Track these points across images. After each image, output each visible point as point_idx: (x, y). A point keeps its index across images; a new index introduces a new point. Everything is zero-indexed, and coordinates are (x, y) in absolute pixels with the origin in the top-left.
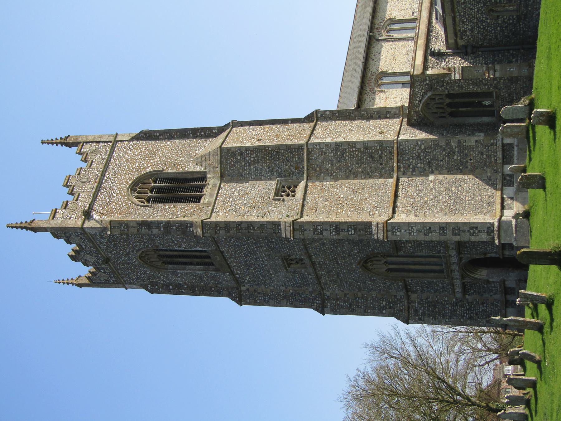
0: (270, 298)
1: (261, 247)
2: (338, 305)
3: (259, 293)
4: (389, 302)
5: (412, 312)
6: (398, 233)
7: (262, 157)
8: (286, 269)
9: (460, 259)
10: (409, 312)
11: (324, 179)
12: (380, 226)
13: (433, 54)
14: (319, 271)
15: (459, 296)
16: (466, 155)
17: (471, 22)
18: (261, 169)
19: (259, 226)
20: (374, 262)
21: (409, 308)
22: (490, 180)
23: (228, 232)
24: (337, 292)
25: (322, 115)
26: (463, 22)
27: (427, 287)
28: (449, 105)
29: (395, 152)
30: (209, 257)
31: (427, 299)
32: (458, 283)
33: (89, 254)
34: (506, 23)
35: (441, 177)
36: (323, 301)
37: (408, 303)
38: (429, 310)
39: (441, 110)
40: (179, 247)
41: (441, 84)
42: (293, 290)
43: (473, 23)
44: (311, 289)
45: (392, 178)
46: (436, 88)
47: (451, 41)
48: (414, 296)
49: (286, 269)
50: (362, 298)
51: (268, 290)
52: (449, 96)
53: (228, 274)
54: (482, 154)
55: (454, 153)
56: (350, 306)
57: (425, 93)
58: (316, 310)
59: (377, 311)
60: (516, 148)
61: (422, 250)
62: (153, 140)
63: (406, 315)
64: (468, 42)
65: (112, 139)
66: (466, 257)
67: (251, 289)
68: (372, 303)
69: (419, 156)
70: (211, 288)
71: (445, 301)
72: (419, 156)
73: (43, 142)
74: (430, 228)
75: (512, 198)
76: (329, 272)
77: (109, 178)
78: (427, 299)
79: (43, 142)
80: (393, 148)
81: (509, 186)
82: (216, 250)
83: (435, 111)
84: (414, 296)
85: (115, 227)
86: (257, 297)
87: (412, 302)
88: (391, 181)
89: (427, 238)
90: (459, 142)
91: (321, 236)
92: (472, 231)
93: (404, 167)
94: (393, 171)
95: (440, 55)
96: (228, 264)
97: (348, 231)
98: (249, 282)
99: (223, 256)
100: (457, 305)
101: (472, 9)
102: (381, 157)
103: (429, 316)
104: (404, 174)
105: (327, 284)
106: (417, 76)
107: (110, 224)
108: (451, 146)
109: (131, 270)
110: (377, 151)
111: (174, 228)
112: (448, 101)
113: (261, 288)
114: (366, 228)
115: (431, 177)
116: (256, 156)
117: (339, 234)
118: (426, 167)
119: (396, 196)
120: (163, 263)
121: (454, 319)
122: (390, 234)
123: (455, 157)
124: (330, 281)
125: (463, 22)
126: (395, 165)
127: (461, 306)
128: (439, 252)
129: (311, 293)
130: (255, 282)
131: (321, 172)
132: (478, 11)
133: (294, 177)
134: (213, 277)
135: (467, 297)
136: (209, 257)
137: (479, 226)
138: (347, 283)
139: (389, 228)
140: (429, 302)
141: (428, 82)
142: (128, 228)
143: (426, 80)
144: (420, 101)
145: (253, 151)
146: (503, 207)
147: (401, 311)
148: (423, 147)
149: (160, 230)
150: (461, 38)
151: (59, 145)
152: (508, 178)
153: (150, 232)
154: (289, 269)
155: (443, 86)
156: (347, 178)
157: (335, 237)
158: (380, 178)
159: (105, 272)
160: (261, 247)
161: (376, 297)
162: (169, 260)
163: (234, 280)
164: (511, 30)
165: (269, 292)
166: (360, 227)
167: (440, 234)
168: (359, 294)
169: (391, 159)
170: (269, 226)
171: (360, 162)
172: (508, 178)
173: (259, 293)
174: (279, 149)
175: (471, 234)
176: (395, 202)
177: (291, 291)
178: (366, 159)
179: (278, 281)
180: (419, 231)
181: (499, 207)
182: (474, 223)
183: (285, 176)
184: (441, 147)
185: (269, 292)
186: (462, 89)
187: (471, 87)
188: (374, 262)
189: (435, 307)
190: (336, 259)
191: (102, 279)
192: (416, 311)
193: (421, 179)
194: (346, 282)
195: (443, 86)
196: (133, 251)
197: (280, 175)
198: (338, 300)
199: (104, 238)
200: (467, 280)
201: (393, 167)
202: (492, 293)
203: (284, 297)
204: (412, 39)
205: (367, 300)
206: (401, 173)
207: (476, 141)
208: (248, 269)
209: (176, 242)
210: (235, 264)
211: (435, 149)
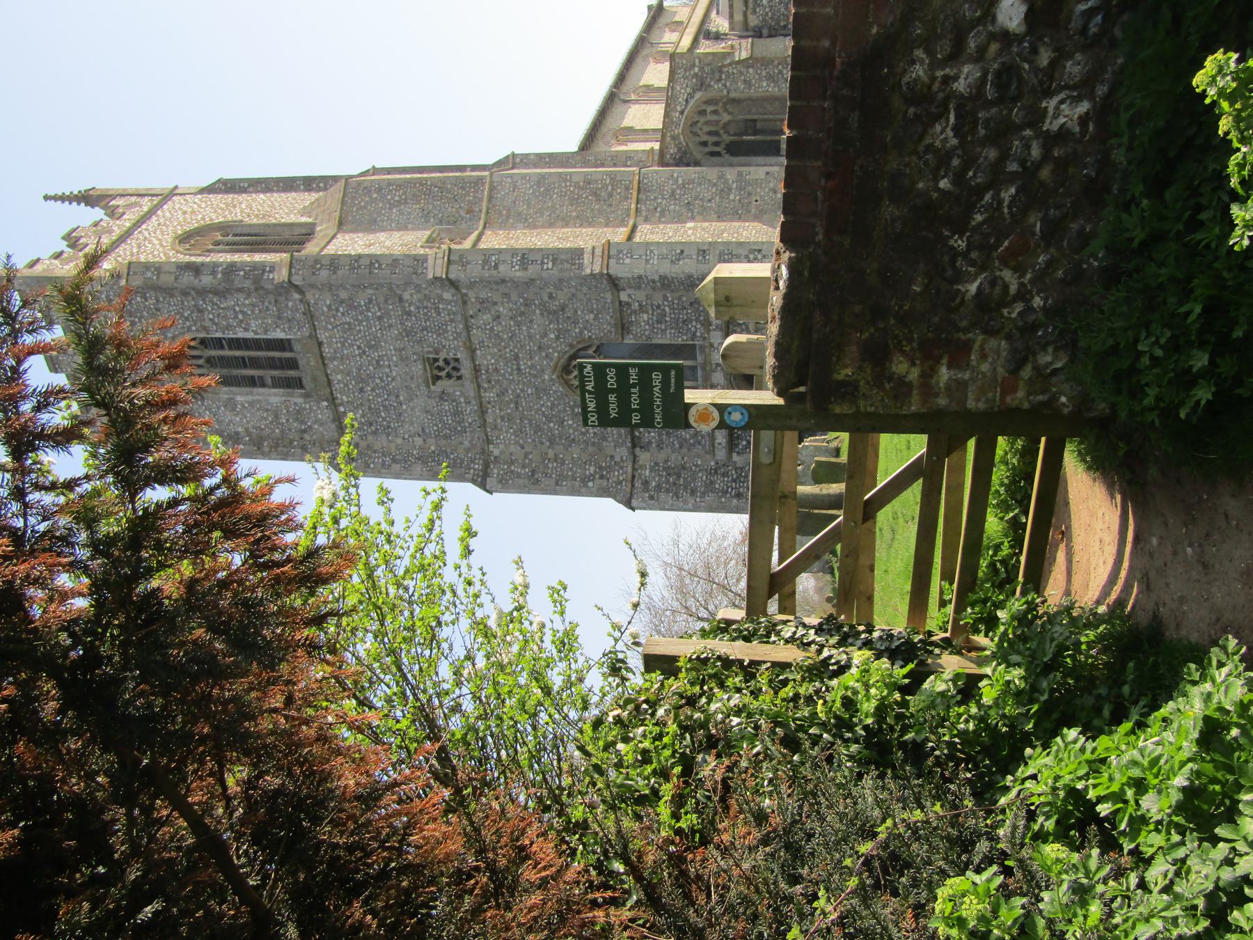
0: (394, 461)
1: (390, 326)
2: (512, 472)
3: (375, 452)
4: (601, 468)
5: (638, 484)
6: (627, 261)
7: (414, 195)
8: (428, 387)
10: (633, 486)
11: (514, 227)
12: (598, 251)
14: (485, 390)
15: (721, 454)
16: (750, 194)
18: (410, 214)
19: (390, 261)
21: (633, 477)
23: (335, 273)
24: (512, 448)
25: (522, 161)
29: (636, 187)
31: (666, 461)
36: (486, 466)
37: (634, 469)
38: (667, 482)
39: (715, 139)
41: (717, 75)
42: (437, 445)
45: (626, 226)
46: (709, 86)
47: (738, 17)
48: (644, 457)
49: (428, 387)
50: (555, 460)
51: (393, 446)
53: (325, 403)
54: (775, 192)
55: (730, 189)
56: (533, 475)
57: (691, 96)
58: (474, 482)
59: (577, 484)
61: (664, 331)
62: (235, 193)
63: (628, 490)
64: (764, 20)
68: (571, 469)
69: (673, 194)
70: (291, 441)
71: (697, 466)
72: (673, 194)
73: (47, 198)
74: (682, 252)
76: (503, 393)
78: (666, 461)
79: (47, 198)
80: (631, 182)
82: (310, 336)
83: (705, 138)
84: (644, 457)
85: (135, 273)
86: (370, 457)
87: (641, 467)
90: (740, 174)
93: (648, 210)
94: (628, 216)
95: (717, 37)
96: (327, 375)
97: (543, 263)
99: (321, 353)
100: (716, 473)
102: (610, 195)
103: (668, 491)
104: (646, 220)
105: (495, 427)
106: (682, 55)
107: (129, 268)
108: (726, 181)
110: (605, 186)
111: (242, 273)
113: (381, 442)
115: (690, 225)
116: (405, 193)
117: (526, 269)
118: (684, 210)
121: (710, 498)
122: (612, 262)
123: (732, 197)
124: (502, 418)
126: (633, 206)
127: (724, 475)
129: (468, 450)
130: (371, 424)
131: (508, 217)
133: (464, 226)
134: (299, 414)
135: (735, 457)
137: (764, 247)
138: (531, 425)
139: (613, 252)
140: (669, 468)
141: (696, 70)
143: (694, 66)
144: (682, 113)
145: (400, 186)
147: (620, 483)
148: (680, 181)
149: (215, 277)
150: (754, 12)
151: (75, 204)
154: (433, 388)
155: (720, 80)
156: (551, 225)
157: (518, 274)
158: (607, 226)
160: (390, 326)
161: (579, 458)
163: (334, 420)
166: (563, 257)
168: (551, 454)
169: (626, 198)
170: (407, 263)
171: (574, 201)
173: (375, 452)
174: (444, 183)
177: (433, 448)
179: (412, 423)
180: (663, 257)
182: (755, 243)
183: (449, 224)
186: (750, 88)
187: (765, 84)
189: (679, 477)
190: (517, 357)
192: (646, 483)
193: (674, 226)
198: (512, 462)
201: (629, 210)
203: (419, 459)
205: (563, 463)
206: (640, 219)
209: (240, 317)
210: (339, 377)
211: (700, 184)
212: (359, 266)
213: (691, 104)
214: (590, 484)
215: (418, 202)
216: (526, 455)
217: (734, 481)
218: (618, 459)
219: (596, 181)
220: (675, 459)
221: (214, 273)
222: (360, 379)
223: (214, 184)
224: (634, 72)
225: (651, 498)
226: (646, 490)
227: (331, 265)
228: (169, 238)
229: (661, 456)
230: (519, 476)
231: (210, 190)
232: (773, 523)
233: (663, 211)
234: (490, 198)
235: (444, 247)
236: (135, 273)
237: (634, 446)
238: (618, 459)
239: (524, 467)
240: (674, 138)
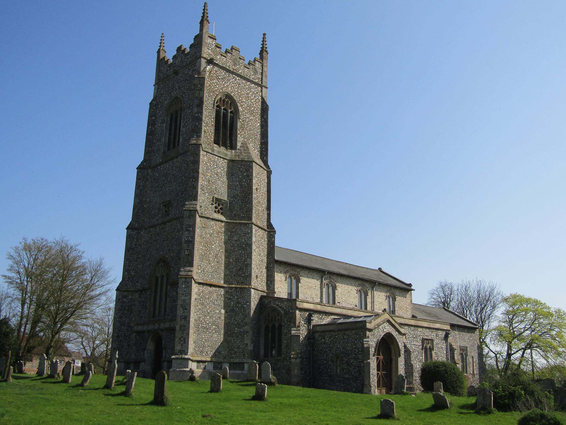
0: (141, 190)
3: (145, 182)
4: (133, 277)
5: (125, 293)
6: (184, 286)
7: (244, 191)
9: (162, 330)
13: (310, 316)
15: (135, 328)
16: (237, 337)
21: (128, 291)
22: (219, 353)
27: (143, 305)
29: (243, 286)
32: (145, 328)
35: (223, 318)
37: (132, 291)
43: (330, 344)
45: (224, 283)
46: (286, 317)
48: (137, 295)
54: (238, 348)
55: (240, 328)
57: (283, 309)
60: (240, 372)
62: (261, 113)
65: (264, 84)
68: (133, 265)
69: (239, 303)
70: (151, 147)
71: (132, 318)
72: (239, 303)
73: (264, 34)
74: (186, 309)
75: (205, 368)
77: (236, 80)
79: (264, 34)
81: (214, 367)
84: (137, 295)
85: (200, 81)
88: (222, 282)
89: (179, 307)
90: (247, 332)
91: (185, 230)
93: (231, 292)
97: (187, 250)
102: (239, 276)
104: (226, 292)
110: (244, 273)
112: (277, 325)
115: (223, 311)
116: (246, 187)
117: (185, 243)
119: (211, 285)
123: (236, 329)
126: (234, 286)
132: (337, 348)
133: (228, 213)
135: (134, 334)
144: (278, 305)
145: (249, 184)
146: (198, 362)
147: (126, 286)
149: (196, 113)
150: (319, 336)
151: (261, 46)
152: (219, 366)
153: (194, 106)
157: (183, 240)
159: (167, 71)
166: (190, 258)
168: (140, 256)
172: (219, 366)
173: (145, 182)
175: (180, 338)
178: (239, 265)
181: (199, 359)
191: (163, 68)
192: (126, 297)
193: (222, 304)
194: (150, 247)
195: (288, 322)
197: (230, 203)
198: (137, 240)
201: (232, 284)
204: (321, 301)
206: (227, 289)
207: (247, 344)
212: (194, 173)
213: (279, 309)
215: (240, 193)
216: (140, 245)
217: (125, 334)
218: (136, 284)
219: (247, 269)
221: (198, 113)
223: (266, 103)
224: (339, 279)
228: (229, 90)
231: (264, 102)
232: (116, 351)
233: (230, 299)
234: (241, 224)
236: (200, 81)
237: (140, 291)
238: (136, 284)
240: (270, 302)
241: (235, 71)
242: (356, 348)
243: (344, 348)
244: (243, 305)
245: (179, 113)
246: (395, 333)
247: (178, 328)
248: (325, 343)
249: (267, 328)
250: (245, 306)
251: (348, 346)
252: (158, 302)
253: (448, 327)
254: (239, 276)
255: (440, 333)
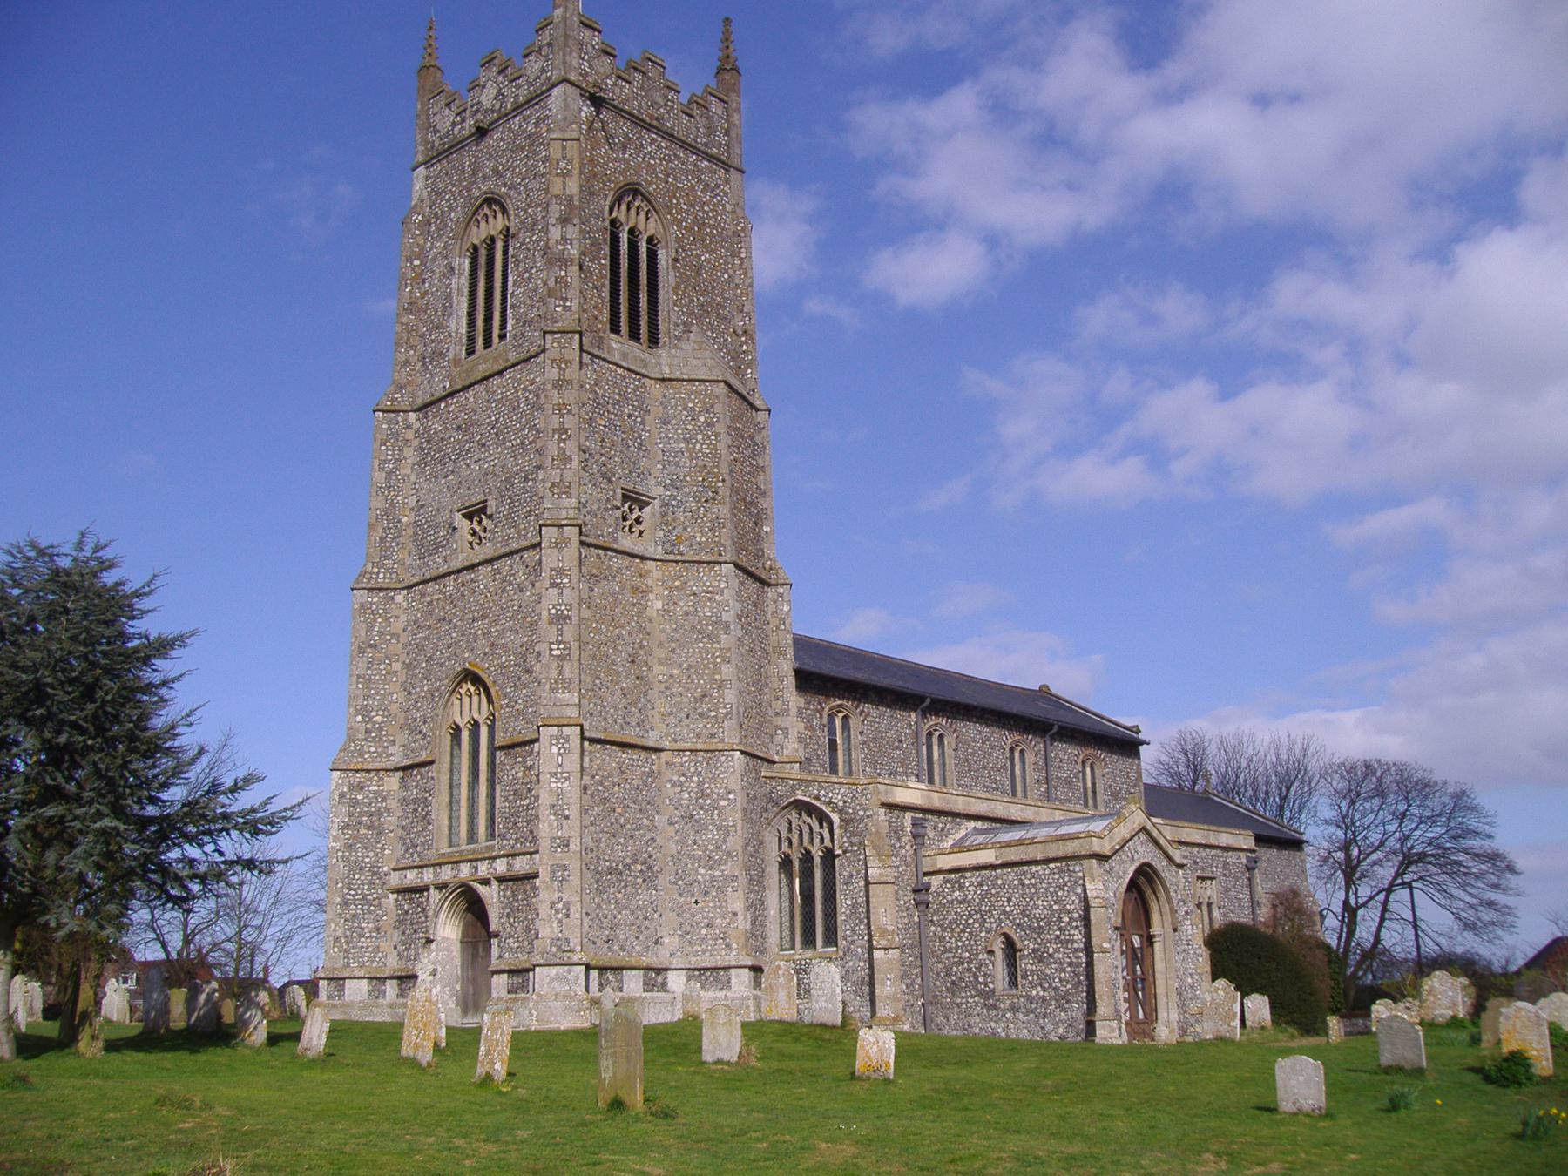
0: (389, 474)
4: (381, 729)
6: (555, 749)
15: (395, 880)
17: (982, 900)
20: (475, 698)
21: (368, 771)
23: (554, 387)
24: (403, 618)
26: (980, 884)
27: (416, 810)
28: (807, 858)
30: (488, 343)
31: (388, 811)
32: (428, 876)
33: (499, 93)
34: (978, 969)
38: (361, 814)
40: (515, 282)
43: (979, 904)
44: (408, 561)
48: (393, 781)
52: (829, 857)
55: (711, 868)
59: (360, 702)
60: (721, 994)
65: (735, 162)
66: (491, 895)
67: (410, 434)
69: (703, 795)
71: (383, 849)
72: (703, 795)
77: (659, 148)
78: (388, 811)
81: (645, 984)
87: (381, 779)
89: (544, 811)
91: (547, 584)
92: (560, 906)
96: (472, 385)
97: (559, 643)
98: (426, 430)
100: (374, 874)
101: (1009, 900)
102: (701, 715)
103: (351, 815)
105: (423, 595)
109: (459, 180)
112: (817, 854)
114: (564, 680)
116: (705, 455)
120: (475, 248)
123: (701, 871)
124: (430, 603)
125: (980, 884)
126: (687, 745)
128: (503, 837)
130: (428, 442)
132: (1004, 912)
136: (488, 343)
140: (380, 815)
142: (564, 175)
144: (817, 798)
147: (361, 755)
152: (660, 979)
153: (552, 220)
159: (454, 124)
161: (392, 702)
162: (482, 260)
164: (962, 979)
165: (403, 472)
167: (553, 839)
172: (660, 979)
175: (552, 905)
176: (613, 743)
178: (698, 685)
184: (725, 841)
185: (403, 472)
188: (475, 698)
189: (368, 828)
190: (484, 617)
191: (437, 118)
192: (361, 788)
194: (428, 638)
195: (852, 844)
196: (505, 185)
198: (387, 620)
199: (537, 125)
200: (435, 896)
202: (400, 948)
207: (735, 914)
208: (459, 428)
214: (359, 718)
217: (364, 898)
220: (390, 821)
222: (470, 424)
225: (342, 796)
226: (352, 788)
227: (564, 381)
229: (393, 803)
230: (370, 629)
233: (681, 784)
235: (656, 491)
236: (564, 148)
238: (391, 749)
239: (381, 634)
241: (655, 123)
242: (1064, 910)
243: (1023, 913)
244: (716, 801)
245: (499, 245)
246: (1160, 864)
247: (544, 874)
248: (964, 901)
249: (786, 864)
250: (723, 803)
251: (1036, 907)
252: (1018, 779)
253: (1247, 841)
254: (701, 715)
255: (1232, 857)
